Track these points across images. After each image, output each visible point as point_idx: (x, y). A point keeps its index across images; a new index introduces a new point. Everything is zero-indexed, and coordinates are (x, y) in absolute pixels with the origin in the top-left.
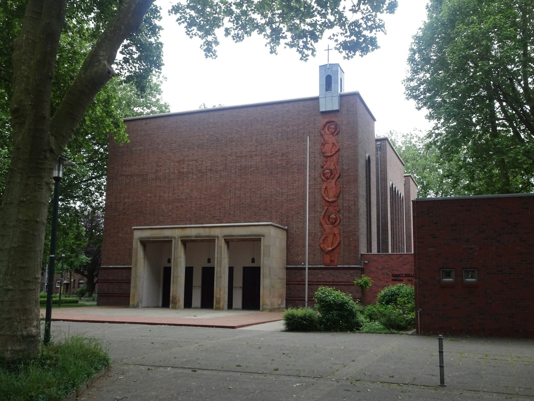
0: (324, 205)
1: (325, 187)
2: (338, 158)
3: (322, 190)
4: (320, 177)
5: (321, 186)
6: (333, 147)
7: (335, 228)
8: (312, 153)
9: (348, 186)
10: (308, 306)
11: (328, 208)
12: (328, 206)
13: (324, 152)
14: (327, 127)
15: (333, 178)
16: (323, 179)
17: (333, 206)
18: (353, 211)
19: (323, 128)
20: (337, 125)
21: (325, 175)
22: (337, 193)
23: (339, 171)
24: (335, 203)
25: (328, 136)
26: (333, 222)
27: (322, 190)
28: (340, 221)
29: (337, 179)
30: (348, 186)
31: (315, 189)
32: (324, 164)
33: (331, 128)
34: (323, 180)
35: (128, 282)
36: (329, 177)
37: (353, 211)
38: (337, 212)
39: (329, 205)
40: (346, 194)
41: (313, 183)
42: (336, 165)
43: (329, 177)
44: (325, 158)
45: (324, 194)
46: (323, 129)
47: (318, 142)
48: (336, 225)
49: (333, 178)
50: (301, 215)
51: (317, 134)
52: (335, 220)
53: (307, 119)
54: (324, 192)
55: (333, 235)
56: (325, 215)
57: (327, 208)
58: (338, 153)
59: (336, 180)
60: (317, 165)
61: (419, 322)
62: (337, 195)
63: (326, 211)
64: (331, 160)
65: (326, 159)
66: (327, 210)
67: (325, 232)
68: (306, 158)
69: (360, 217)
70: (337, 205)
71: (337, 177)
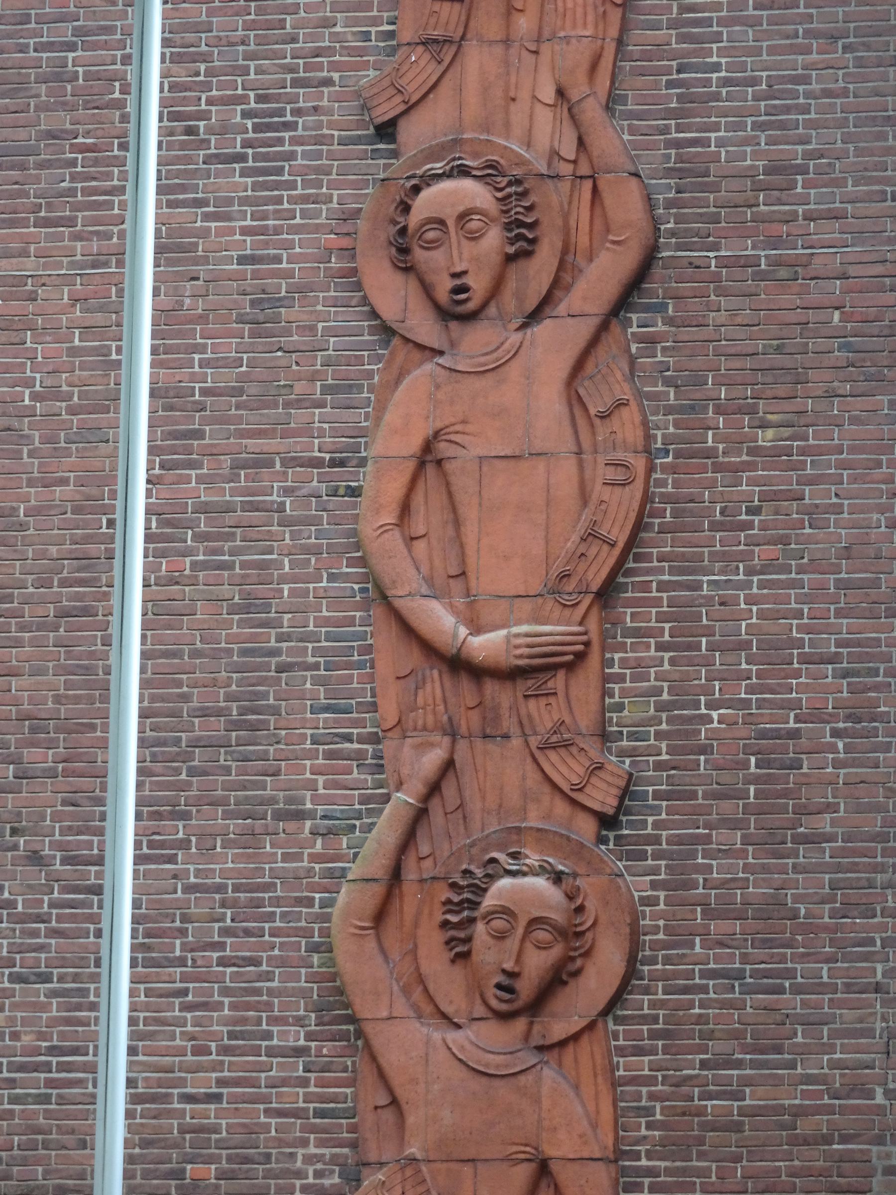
0: (389, 712)
1: (414, 444)
3: (366, 478)
4: (595, 445)
5: (359, 417)
7: (548, 1073)
9: (766, 438)
10: (130, 1093)
11: (449, 765)
12: (452, 732)
15: (547, 301)
16: (389, 311)
17: (525, 727)
18: (824, 823)
21: (419, 254)
22: (591, 535)
24: (558, 681)
26: (526, 988)
27: (366, 478)
28: (631, 973)
29: (604, 327)
30: (766, 438)
31: (262, 462)
32: (413, 88)
34: (387, 331)
37: (824, 823)
38: (586, 828)
39: (470, 721)
40: (727, 559)
42: (592, 111)
43: (479, 283)
45: (395, 538)
48: (559, 1030)
49: (547, 301)
50: (35, 858)
52: (557, 952)
54: (405, 509)
55: (522, 1173)
56: (410, 874)
57: (433, 759)
59: (584, 330)
60: (304, 98)
61: (810, 1087)
62: (597, 578)
63: (420, 815)
66: (434, 788)
68: (160, 554)
70: (585, 721)
71: (611, 290)
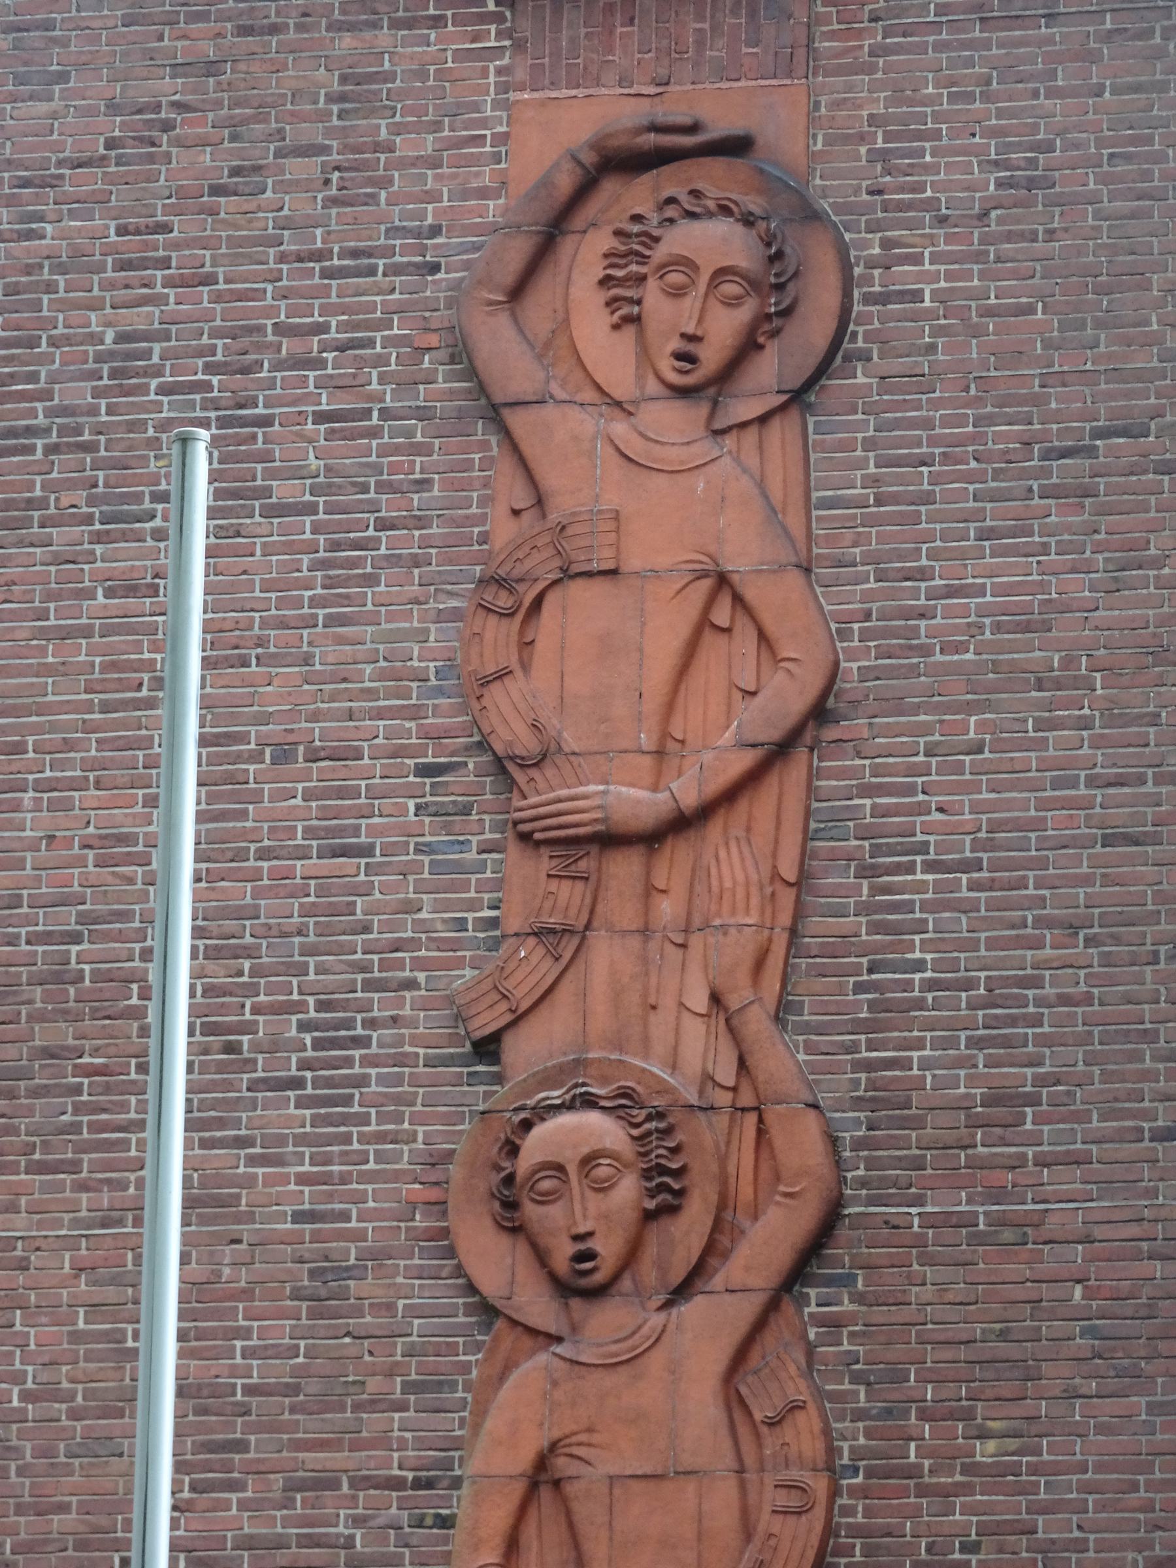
1: (523, 1459)
2: (802, 883)
3: (461, 1504)
5: (452, 1424)
6: (713, 648)
8: (284, 755)
9: (985, 1451)
13: (527, 744)
14: (602, 241)
16: (491, 1285)
19: (517, 253)
20: (812, 216)
21: (531, 1211)
23: (811, 1126)
25: (620, 428)
27: (461, 1504)
29: (773, 1306)
30: (985, 1451)
31: (325, 1483)
32: (523, 991)
33: (687, 264)
34: (488, 1311)
35: (125, 1505)
36: (608, 1248)
41: (280, 1371)
42: (757, 1023)
43: (608, 1248)
44: (545, 863)
46: (517, 292)
47: (411, 542)
51: (405, 385)
53: (212, 68)
55: (706, 584)
58: (796, 771)
60: (380, 1005)
64: (667, 909)
65: (570, 894)
67: (667, 1305)
69: (750, 1379)
